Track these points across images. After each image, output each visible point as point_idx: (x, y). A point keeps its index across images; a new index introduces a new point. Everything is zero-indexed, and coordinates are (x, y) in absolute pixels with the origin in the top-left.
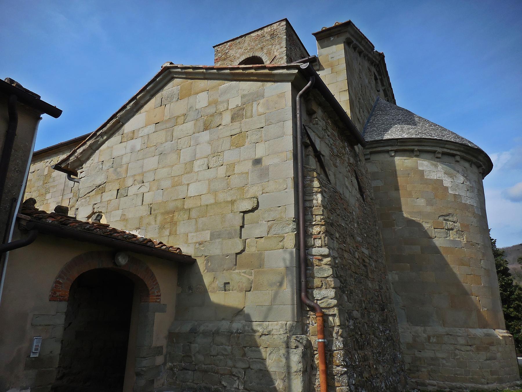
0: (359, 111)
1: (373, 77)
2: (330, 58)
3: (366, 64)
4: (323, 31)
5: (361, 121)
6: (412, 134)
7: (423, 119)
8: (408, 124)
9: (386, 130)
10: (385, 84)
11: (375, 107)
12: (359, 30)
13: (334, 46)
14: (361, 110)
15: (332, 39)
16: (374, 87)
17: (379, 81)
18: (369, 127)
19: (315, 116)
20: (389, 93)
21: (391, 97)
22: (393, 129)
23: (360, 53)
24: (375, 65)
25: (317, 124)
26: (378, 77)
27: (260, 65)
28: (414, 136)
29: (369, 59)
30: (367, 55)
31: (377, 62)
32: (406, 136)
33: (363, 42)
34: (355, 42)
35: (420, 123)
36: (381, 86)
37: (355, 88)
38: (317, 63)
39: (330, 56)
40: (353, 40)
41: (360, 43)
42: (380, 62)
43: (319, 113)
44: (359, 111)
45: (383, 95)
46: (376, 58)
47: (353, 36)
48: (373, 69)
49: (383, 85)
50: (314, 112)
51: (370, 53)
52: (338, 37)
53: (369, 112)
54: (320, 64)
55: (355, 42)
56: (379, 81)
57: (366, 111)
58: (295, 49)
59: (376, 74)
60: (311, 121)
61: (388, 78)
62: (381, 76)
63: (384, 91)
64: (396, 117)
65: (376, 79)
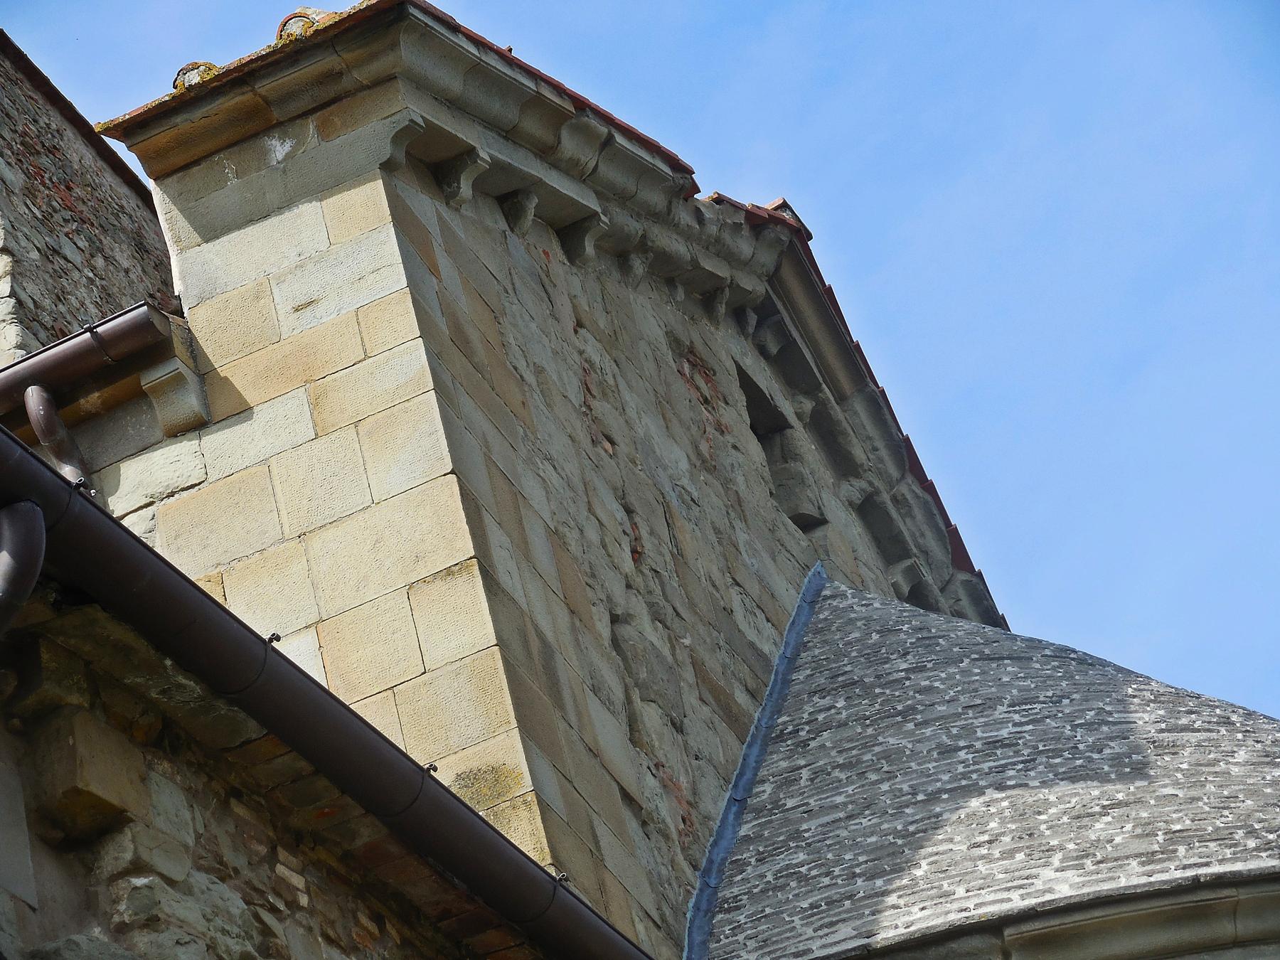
0: (633, 724)
1: (737, 415)
2: (284, 308)
3: (652, 315)
4: (186, 101)
5: (666, 811)
6: (1119, 860)
7: (1200, 703)
8: (1073, 777)
9: (892, 859)
10: (859, 453)
11: (791, 663)
12: (506, 57)
13: (308, 212)
14: (651, 716)
15: (279, 149)
16: (757, 495)
17: (802, 439)
18: (748, 855)
19: (120, 851)
20: (910, 527)
21: (939, 552)
22: (951, 841)
23: (569, 230)
24: (738, 315)
25: (152, 923)
26: (786, 407)
27: (774, 297)
28: (1132, 877)
29: (668, 273)
30: (643, 245)
31: (753, 285)
32: (1064, 886)
33: (570, 145)
34: (488, 149)
35: (1174, 750)
36: (827, 476)
37: (555, 535)
38: (178, 365)
39: (284, 297)
40: (468, 133)
41: (546, 153)
42: (774, 279)
43: (167, 815)
44: (633, 724)
45: (867, 552)
46: (729, 257)
47: (455, 105)
48: (729, 347)
49: (844, 466)
50: (113, 821)
51: (663, 218)
52: (325, 132)
53: (734, 719)
54: (205, 373)
55: (488, 149)
56: (802, 439)
57: (699, 713)
58: (96, 249)
59: (765, 379)
60: (88, 908)
61: (879, 404)
62: (811, 390)
63: (867, 509)
64: (969, 731)
65: (768, 425)
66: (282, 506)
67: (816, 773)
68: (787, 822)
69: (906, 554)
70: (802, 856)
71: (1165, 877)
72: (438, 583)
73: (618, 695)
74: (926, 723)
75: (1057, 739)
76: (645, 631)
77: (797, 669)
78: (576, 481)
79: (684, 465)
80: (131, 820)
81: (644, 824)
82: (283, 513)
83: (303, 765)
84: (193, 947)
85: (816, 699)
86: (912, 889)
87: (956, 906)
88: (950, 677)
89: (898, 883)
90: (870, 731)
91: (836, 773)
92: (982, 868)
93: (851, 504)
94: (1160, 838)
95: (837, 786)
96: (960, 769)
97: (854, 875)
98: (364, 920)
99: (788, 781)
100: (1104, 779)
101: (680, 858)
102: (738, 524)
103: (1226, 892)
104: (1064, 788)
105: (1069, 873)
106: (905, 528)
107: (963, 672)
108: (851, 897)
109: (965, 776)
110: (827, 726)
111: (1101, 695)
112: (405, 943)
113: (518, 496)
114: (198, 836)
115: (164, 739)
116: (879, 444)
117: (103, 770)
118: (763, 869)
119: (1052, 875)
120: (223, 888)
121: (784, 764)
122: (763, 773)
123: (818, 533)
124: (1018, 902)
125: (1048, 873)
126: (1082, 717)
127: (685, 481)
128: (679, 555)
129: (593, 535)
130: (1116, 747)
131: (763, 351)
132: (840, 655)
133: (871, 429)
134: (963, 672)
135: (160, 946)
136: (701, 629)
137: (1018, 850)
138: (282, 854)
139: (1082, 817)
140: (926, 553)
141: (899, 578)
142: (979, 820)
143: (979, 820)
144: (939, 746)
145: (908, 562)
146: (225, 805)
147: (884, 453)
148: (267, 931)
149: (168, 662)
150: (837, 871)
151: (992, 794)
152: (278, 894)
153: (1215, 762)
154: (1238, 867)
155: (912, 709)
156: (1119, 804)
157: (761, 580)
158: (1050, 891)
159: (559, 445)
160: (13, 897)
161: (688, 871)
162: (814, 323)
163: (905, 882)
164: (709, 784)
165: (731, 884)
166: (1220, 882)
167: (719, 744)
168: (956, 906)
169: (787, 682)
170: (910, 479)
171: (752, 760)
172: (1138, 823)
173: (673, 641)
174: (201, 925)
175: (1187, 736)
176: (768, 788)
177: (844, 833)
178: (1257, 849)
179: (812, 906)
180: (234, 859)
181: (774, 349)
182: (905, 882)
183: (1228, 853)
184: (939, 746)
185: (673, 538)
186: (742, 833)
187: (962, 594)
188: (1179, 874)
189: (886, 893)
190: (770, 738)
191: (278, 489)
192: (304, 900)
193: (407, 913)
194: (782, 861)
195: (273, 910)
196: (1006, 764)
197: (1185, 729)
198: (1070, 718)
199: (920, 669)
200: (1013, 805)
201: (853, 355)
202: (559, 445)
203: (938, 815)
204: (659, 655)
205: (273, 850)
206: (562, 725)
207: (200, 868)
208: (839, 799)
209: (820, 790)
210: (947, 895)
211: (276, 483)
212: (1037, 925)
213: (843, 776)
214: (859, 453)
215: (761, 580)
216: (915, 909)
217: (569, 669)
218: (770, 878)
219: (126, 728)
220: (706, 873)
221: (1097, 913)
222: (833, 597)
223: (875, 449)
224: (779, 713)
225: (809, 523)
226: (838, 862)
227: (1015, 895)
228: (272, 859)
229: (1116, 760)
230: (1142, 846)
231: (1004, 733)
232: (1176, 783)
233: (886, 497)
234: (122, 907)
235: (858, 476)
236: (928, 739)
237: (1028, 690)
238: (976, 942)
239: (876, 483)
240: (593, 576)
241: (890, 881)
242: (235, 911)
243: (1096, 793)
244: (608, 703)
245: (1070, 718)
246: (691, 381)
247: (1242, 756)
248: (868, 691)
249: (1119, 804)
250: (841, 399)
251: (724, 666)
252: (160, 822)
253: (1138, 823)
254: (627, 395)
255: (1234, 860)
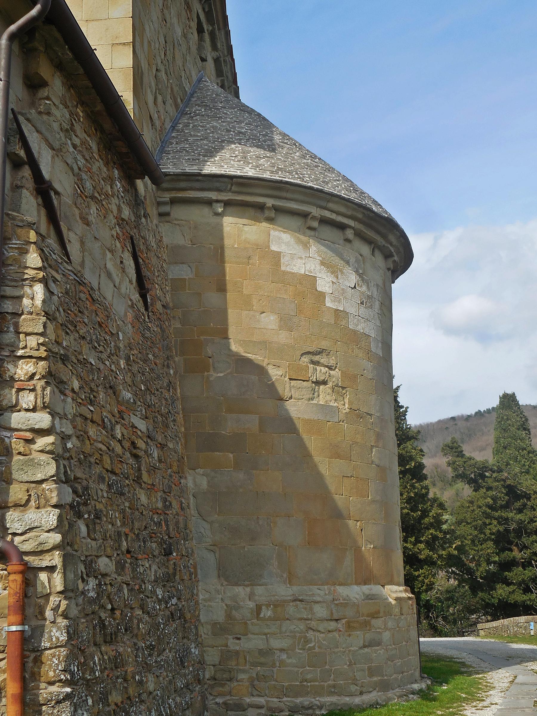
5: (157, 123)
6: (265, 170)
7: (290, 139)
9: (211, 153)
11: (192, 95)
14: (160, 98)
19: (44, 92)
20: (226, 69)
22: (225, 153)
25: (49, 114)
26: (205, 27)
28: (267, 175)
32: (251, 173)
35: (283, 148)
36: (210, 49)
43: (56, 86)
45: (214, 72)
49: (214, 47)
50: (44, 84)
53: (177, 106)
57: (170, 101)
60: (32, 104)
62: (212, 24)
63: (217, 61)
64: (234, 127)
65: (200, 30)
66: (83, 11)
67: (194, 126)
68: (185, 136)
69: (223, 76)
70: (187, 146)
71: (275, 178)
72: (121, 46)
73: (154, 91)
74: (224, 122)
75: (256, 136)
76: (163, 75)
77: (193, 97)
78: (157, 29)
79: (180, 34)
80: (48, 85)
81: (152, 125)
82: (83, 13)
83: (90, 85)
84: (57, 123)
85: (197, 107)
86: (214, 162)
87: (224, 170)
88: (232, 112)
89: (210, 160)
90: (210, 119)
91: (199, 127)
92: (232, 162)
93: (213, 58)
94: (276, 168)
95: (199, 131)
96: (231, 136)
97: (200, 155)
98: (93, 129)
99: (187, 125)
100: (265, 150)
101: (158, 137)
102: (188, 55)
103: (287, 186)
104: (255, 149)
105: (253, 170)
106: (225, 69)
107: (235, 112)
108: (198, 160)
109: (231, 138)
110: (198, 115)
111: (268, 129)
112: (100, 138)
113: (144, 29)
114: (63, 95)
115: (59, 66)
116: (225, 45)
117: (45, 70)
118: (177, 146)
119: (249, 169)
120: (65, 110)
121: (186, 121)
122: (180, 121)
123: (204, 63)
124: (239, 173)
125: (247, 168)
126: (260, 132)
127: (179, 39)
128: (174, 58)
129: (157, 46)
130: (269, 143)
131: (204, 9)
132: (204, 97)
133: (224, 40)
134: (235, 112)
135: (49, 120)
136: (175, 79)
137: (242, 161)
138: (79, 106)
139: (258, 157)
140: (227, 77)
141: (219, 81)
142: (234, 151)
143: (234, 151)
144: (226, 129)
145: (222, 78)
146: (69, 88)
147: (225, 47)
148: (72, 124)
149: (67, 47)
150: (196, 152)
151: (237, 145)
152: (76, 116)
153: (291, 154)
154: (292, 181)
155: (221, 117)
156: (268, 157)
157: (190, 71)
158: (247, 173)
159: (155, 18)
160: (16, 96)
161: (159, 140)
162: (219, 7)
163: (213, 160)
164: (168, 120)
165: (168, 147)
166: (287, 183)
167: (171, 110)
168: (224, 170)
169: (190, 100)
170: (229, 56)
171: (178, 117)
172: (271, 163)
173: (168, 80)
174: (59, 118)
175: (286, 145)
176: (181, 126)
177: (199, 143)
178: (297, 178)
179: (188, 159)
180: (69, 104)
181: (207, 10)
182: (213, 160)
183: (291, 176)
184: (226, 129)
185: (174, 52)
186: (173, 135)
187: (233, 90)
188: (278, 178)
189: (207, 161)
190: (183, 113)
191: (84, 6)
192: (82, 120)
193: (102, 131)
194: (182, 145)
195: (75, 120)
196: (241, 138)
197: (285, 143)
198: (259, 132)
199: (225, 108)
200: (242, 149)
201: (225, 18)
202: (155, 18)
203: (224, 146)
204: (164, 83)
205: (77, 104)
206: (141, 94)
207: (61, 103)
208: (199, 134)
209: (194, 131)
210: (222, 166)
211: (83, 4)
212: (242, 180)
213: (201, 129)
214: (219, 45)
215: (190, 71)
216: (214, 167)
217: (146, 80)
218: (178, 148)
219: (51, 60)
220: (163, 142)
221: (256, 181)
222: (205, 81)
223: (223, 45)
224: (187, 107)
225: (203, 60)
226: (197, 150)
227: (238, 171)
228: (77, 107)
229: (269, 146)
230: (271, 169)
231: (243, 131)
232: (282, 156)
233: (222, 59)
234: (42, 107)
235: (217, 51)
236: (224, 126)
237: (250, 121)
238: (226, 180)
239: (221, 55)
240: (155, 57)
241: (209, 159)
242: (67, 117)
243: (262, 152)
244: (152, 91)
245: (259, 132)
246: (186, 12)
247: (298, 154)
248: (210, 109)
249: (268, 157)
250: (219, 29)
251: (177, 91)
252: (55, 88)
253: (271, 163)
254: (172, 11)
255: (291, 179)
